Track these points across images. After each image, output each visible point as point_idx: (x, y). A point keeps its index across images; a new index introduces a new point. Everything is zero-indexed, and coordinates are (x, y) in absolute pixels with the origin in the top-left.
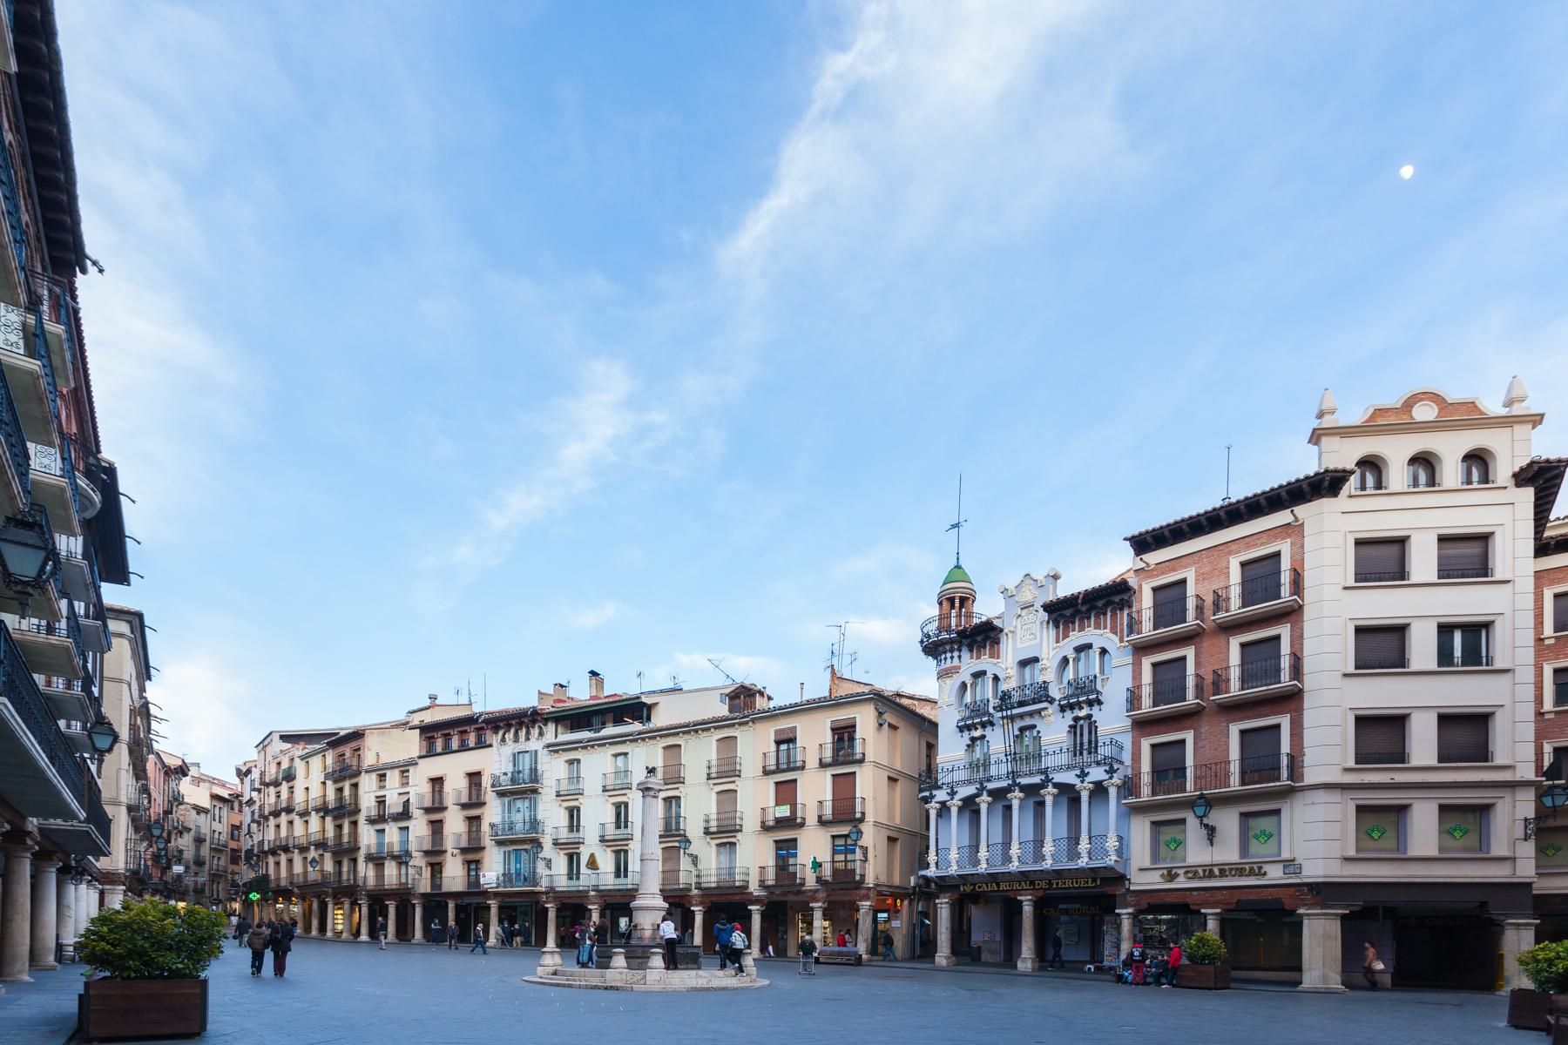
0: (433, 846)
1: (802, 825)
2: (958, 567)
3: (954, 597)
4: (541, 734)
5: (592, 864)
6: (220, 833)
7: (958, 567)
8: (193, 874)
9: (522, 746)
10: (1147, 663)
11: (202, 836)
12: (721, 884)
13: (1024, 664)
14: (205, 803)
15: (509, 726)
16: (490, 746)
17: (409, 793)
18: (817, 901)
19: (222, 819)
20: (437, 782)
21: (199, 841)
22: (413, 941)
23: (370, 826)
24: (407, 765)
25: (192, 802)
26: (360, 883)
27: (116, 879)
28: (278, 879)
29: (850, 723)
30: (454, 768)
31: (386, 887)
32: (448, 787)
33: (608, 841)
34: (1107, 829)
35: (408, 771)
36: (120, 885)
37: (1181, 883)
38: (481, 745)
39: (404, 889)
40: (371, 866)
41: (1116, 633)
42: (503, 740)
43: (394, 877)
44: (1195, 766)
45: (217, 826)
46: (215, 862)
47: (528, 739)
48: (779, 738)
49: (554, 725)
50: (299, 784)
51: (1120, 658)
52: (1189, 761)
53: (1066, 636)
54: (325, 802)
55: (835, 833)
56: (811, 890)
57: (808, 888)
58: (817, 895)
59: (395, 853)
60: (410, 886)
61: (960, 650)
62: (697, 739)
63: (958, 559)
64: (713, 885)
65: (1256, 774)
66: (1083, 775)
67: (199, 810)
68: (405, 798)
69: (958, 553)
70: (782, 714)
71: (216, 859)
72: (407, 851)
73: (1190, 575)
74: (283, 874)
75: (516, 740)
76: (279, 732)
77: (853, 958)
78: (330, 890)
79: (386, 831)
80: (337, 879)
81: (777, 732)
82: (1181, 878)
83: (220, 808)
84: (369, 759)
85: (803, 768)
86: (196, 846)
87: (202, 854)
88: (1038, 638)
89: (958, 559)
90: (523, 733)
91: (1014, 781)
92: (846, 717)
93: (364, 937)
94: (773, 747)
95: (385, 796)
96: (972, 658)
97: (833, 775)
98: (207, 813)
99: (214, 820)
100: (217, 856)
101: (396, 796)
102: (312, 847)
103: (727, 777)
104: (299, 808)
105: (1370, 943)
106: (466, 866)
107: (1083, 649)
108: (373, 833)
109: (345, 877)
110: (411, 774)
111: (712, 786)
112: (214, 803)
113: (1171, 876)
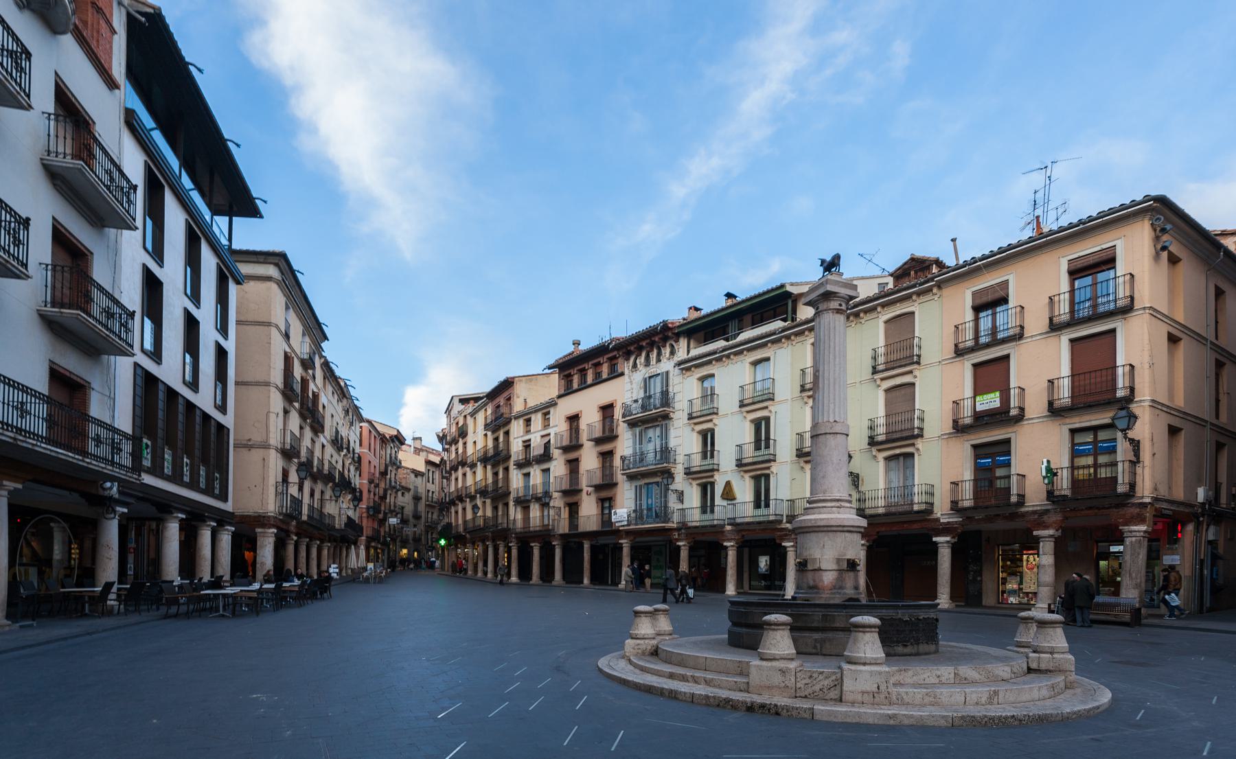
1: (1020, 417)
4: (673, 353)
5: (728, 494)
6: (433, 492)
11: (419, 495)
12: (893, 510)
15: (640, 349)
16: (622, 374)
17: (549, 434)
18: (1046, 527)
20: (574, 419)
21: (417, 499)
23: (518, 470)
25: (411, 467)
27: (266, 522)
29: (1104, 256)
30: (587, 403)
31: (531, 529)
33: (746, 465)
36: (269, 528)
38: (615, 374)
40: (519, 509)
42: (635, 366)
45: (430, 487)
47: (659, 360)
48: (979, 302)
50: (470, 439)
55: (1077, 426)
56: (1034, 512)
57: (1031, 509)
58: (1045, 518)
62: (858, 325)
64: (881, 511)
67: (417, 474)
68: (546, 440)
70: (987, 266)
74: (460, 522)
75: (647, 363)
78: (490, 534)
79: (531, 475)
81: (974, 294)
83: (433, 472)
85: (1019, 336)
87: (419, 509)
93: (514, 579)
94: (969, 315)
95: (530, 440)
99: (429, 481)
101: (539, 439)
102: (478, 496)
103: (901, 366)
106: (600, 504)
108: (520, 477)
110: (551, 416)
111: (878, 382)
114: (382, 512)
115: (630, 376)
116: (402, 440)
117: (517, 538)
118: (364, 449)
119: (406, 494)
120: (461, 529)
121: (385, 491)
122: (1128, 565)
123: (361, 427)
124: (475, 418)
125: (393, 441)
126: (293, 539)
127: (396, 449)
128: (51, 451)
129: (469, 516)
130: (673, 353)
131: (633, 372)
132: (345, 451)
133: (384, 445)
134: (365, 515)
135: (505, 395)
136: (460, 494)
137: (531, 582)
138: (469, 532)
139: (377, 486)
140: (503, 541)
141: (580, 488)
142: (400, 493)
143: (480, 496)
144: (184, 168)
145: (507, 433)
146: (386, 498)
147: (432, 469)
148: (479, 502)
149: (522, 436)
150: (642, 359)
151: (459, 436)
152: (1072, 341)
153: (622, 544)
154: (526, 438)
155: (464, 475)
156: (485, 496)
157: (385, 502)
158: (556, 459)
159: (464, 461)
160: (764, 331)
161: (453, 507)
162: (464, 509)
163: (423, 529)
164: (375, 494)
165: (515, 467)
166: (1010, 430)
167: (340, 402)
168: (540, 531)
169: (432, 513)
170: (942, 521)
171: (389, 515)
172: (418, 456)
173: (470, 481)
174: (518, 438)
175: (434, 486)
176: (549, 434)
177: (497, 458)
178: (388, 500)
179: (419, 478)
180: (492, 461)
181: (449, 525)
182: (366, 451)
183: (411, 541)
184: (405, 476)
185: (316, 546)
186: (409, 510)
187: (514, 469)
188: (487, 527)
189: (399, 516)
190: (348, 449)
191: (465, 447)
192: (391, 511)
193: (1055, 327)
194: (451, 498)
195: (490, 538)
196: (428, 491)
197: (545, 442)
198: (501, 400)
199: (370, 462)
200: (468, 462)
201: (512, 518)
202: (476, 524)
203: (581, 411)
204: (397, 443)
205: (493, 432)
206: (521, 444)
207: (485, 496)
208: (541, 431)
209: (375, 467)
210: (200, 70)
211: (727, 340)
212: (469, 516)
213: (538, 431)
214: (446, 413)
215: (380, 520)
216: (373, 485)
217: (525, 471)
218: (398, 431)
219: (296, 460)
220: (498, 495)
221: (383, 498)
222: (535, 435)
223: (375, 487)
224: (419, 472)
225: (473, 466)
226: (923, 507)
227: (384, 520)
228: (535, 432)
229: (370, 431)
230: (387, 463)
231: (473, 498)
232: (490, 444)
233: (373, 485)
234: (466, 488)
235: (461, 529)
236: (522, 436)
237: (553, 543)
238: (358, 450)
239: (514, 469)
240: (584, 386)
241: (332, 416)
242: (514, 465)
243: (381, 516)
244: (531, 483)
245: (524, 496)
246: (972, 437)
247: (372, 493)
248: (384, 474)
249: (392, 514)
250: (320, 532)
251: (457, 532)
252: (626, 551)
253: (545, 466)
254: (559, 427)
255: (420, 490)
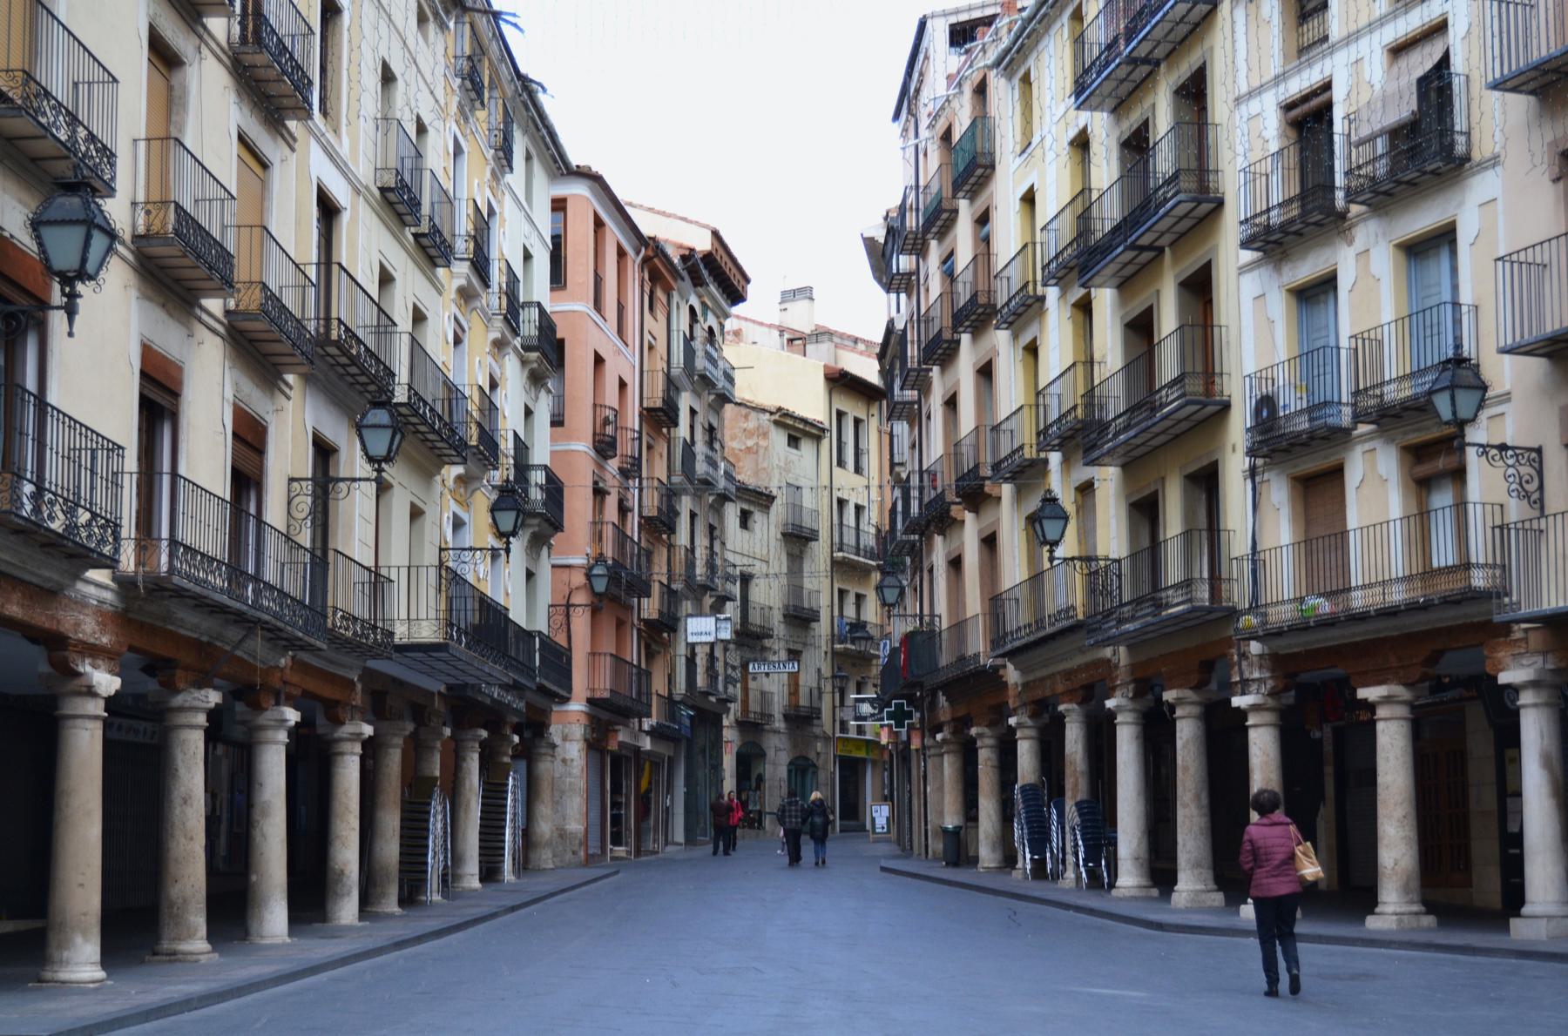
6: (859, 509)
8: (783, 655)
11: (807, 522)
13: (790, 296)
14: (813, 403)
17: (1439, 28)
18: (1013, 713)
19: (864, 463)
21: (797, 539)
22: (1522, 930)
23: (1265, 272)
25: (771, 402)
26: (1238, 594)
31: (1358, 601)
39: (1448, 601)
40: (1278, 493)
43: (1396, 539)
45: (846, 482)
46: (850, 611)
50: (1005, 192)
54: (1090, 393)
59: (1393, 393)
60: (1479, 580)
65: (651, 848)
67: (798, 431)
68: (1422, 61)
71: (851, 600)
72: (1459, 361)
74: (974, 604)
76: (945, 14)
78: (1122, 655)
79: (1344, 283)
80: (1146, 589)
83: (857, 422)
86: (790, 555)
87: (808, 584)
98: (818, 439)
99: (841, 463)
100: (853, 590)
101: (1376, 66)
102: (1055, 458)
108: (1279, 306)
109: (1173, 572)
112: (843, 403)
114: (656, 588)
116: (736, 279)
117: (1277, 662)
118: (574, 299)
119: (758, 517)
120: (978, 643)
121: (670, 494)
123: (559, 205)
124: (1026, 80)
125: (698, 282)
126: (91, 692)
127: (712, 321)
129: (1014, 569)
132: (462, 269)
133: (659, 293)
134: (581, 598)
136: (968, 464)
137: (1372, 923)
138: (1012, 655)
139: (631, 471)
140: (1197, 688)
142: (732, 512)
143: (1066, 461)
144: (647, 423)
145: (1194, 93)
146: (672, 530)
147: (853, 409)
148: (1059, 481)
149: (1279, 79)
151: (957, 186)
154: (1298, 85)
155: (986, 372)
156: (1088, 450)
157: (671, 547)
158: (1495, 161)
159: (982, 300)
161: (938, 540)
162: (990, 542)
163: (827, 671)
164: (623, 510)
165: (1247, 256)
167: (432, 27)
168: (1412, 608)
169: (860, 598)
171: (687, 606)
172: (799, 358)
173: (1011, 391)
174: (1252, 94)
175: (859, 481)
176: (1439, 28)
178: (682, 538)
179: (807, 447)
180: (1121, 255)
182: (585, 306)
183: (779, 724)
184: (750, 443)
185: (283, 736)
186: (768, 595)
187: (1244, 269)
188: (1108, 614)
189: (731, 609)
190: (480, 265)
191: (987, 240)
192: (698, 590)
194: (930, 495)
195: (1122, 675)
196: (842, 503)
197: (1419, 72)
199: (599, 360)
200: (1001, 299)
201: (1238, 543)
202: (1050, 608)
204: (713, 288)
205: (1119, 108)
207: (1088, 450)
209: (623, 385)
210: (514, 15)
212: (1014, 569)
213: (1372, 26)
214: (896, 116)
215: (647, 622)
216: (613, 465)
217: (1306, 269)
218: (716, 235)
219: (214, 305)
221: (660, 525)
222: (1352, 52)
223: (624, 473)
224: (804, 421)
225: (1027, 309)
228: (1351, 38)
229: (599, 224)
230: (675, 372)
231: (1027, 473)
232: (1105, 169)
233: (613, 465)
234: (996, 429)
235: (978, 643)
236: (1279, 79)
237: (1504, 678)
238: (538, 286)
239: (1244, 269)
241: (388, 77)
242: (1246, 244)
243: (650, 607)
244: (1346, 327)
245: (1310, 409)
247: (611, 502)
248: (660, 418)
249: (698, 602)
250: (304, 656)
251: (962, 659)
253: (1421, 220)
255: (808, 501)
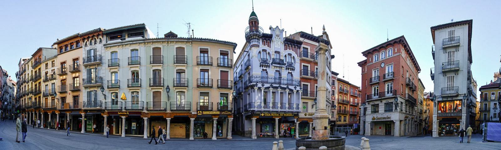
0: (62, 90)
2: (253, 12)
3: (253, 21)
4: (101, 41)
7: (253, 12)
9: (93, 46)
10: (303, 64)
15: (88, 38)
16: (82, 47)
17: (54, 69)
20: (63, 63)
24: (53, 58)
28: (23, 105)
30: (68, 57)
31: (48, 107)
32: (67, 65)
34: (279, 102)
35: (54, 61)
37: (307, 116)
38: (78, 47)
41: (296, 54)
42: (86, 44)
44: (310, 91)
47: (95, 43)
48: (202, 51)
49: (106, 37)
50: (27, 72)
51: (298, 59)
52: (309, 90)
53: (286, 49)
61: (259, 40)
63: (253, 9)
66: (295, 88)
68: (54, 71)
69: (253, 7)
73: (309, 48)
74: (24, 104)
75: (91, 44)
77: (310, 110)
82: (307, 115)
84: (43, 59)
88: (280, 45)
89: (253, 9)
90: (93, 41)
91: (280, 85)
92: (225, 50)
93: (42, 127)
95: (48, 72)
96: (263, 44)
97: (221, 71)
101: (51, 71)
104: (27, 81)
105: (452, 124)
107: (290, 54)
110: (55, 62)
111: (175, 67)
113: (305, 115)
115: (84, 48)
120: (24, 107)
122: (478, 143)
128: (75, 113)
130: (101, 41)
131: (85, 47)
135: (39, 55)
141: (66, 91)
150: (98, 40)
152: (221, 71)
153: (82, 115)
160: (134, 39)
166: (209, 90)
170: (193, 113)
176: (54, 69)
177: (37, 78)
181: (20, 106)
193: (219, 66)
198: (37, 57)
203: (66, 61)
206: (44, 73)
208: (51, 68)
211: (122, 40)
220: (37, 92)
226: (120, 108)
227: (4, 103)
240: (66, 51)
246: (201, 90)
252: (68, 115)
254: (58, 66)
